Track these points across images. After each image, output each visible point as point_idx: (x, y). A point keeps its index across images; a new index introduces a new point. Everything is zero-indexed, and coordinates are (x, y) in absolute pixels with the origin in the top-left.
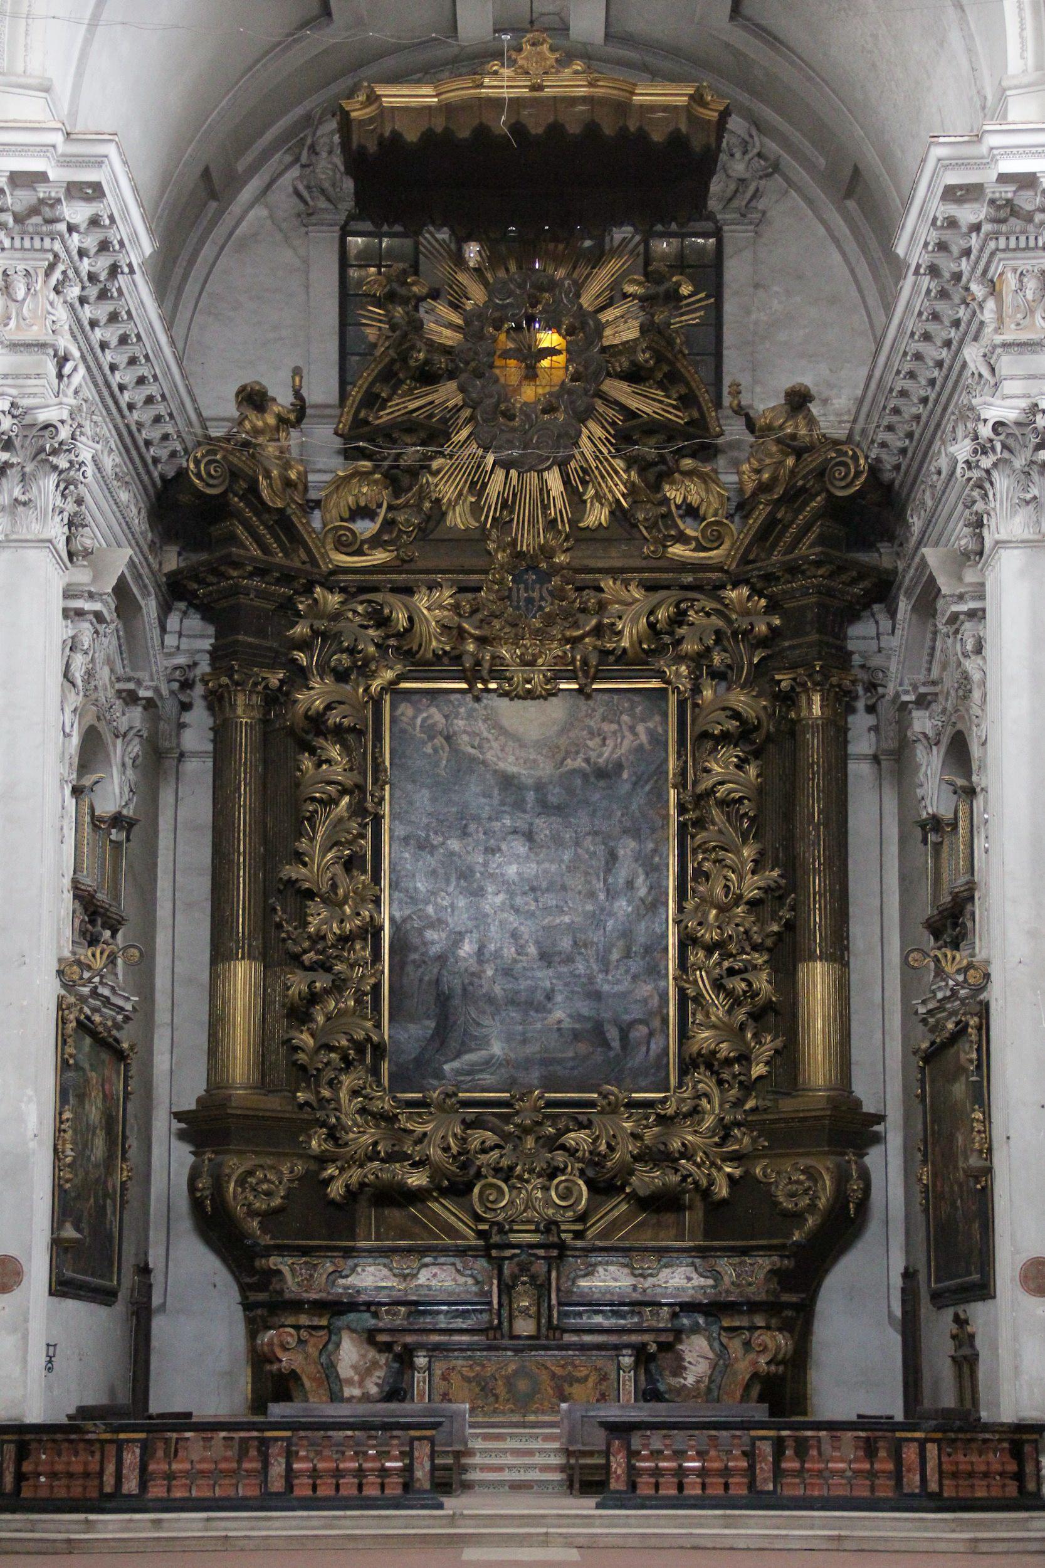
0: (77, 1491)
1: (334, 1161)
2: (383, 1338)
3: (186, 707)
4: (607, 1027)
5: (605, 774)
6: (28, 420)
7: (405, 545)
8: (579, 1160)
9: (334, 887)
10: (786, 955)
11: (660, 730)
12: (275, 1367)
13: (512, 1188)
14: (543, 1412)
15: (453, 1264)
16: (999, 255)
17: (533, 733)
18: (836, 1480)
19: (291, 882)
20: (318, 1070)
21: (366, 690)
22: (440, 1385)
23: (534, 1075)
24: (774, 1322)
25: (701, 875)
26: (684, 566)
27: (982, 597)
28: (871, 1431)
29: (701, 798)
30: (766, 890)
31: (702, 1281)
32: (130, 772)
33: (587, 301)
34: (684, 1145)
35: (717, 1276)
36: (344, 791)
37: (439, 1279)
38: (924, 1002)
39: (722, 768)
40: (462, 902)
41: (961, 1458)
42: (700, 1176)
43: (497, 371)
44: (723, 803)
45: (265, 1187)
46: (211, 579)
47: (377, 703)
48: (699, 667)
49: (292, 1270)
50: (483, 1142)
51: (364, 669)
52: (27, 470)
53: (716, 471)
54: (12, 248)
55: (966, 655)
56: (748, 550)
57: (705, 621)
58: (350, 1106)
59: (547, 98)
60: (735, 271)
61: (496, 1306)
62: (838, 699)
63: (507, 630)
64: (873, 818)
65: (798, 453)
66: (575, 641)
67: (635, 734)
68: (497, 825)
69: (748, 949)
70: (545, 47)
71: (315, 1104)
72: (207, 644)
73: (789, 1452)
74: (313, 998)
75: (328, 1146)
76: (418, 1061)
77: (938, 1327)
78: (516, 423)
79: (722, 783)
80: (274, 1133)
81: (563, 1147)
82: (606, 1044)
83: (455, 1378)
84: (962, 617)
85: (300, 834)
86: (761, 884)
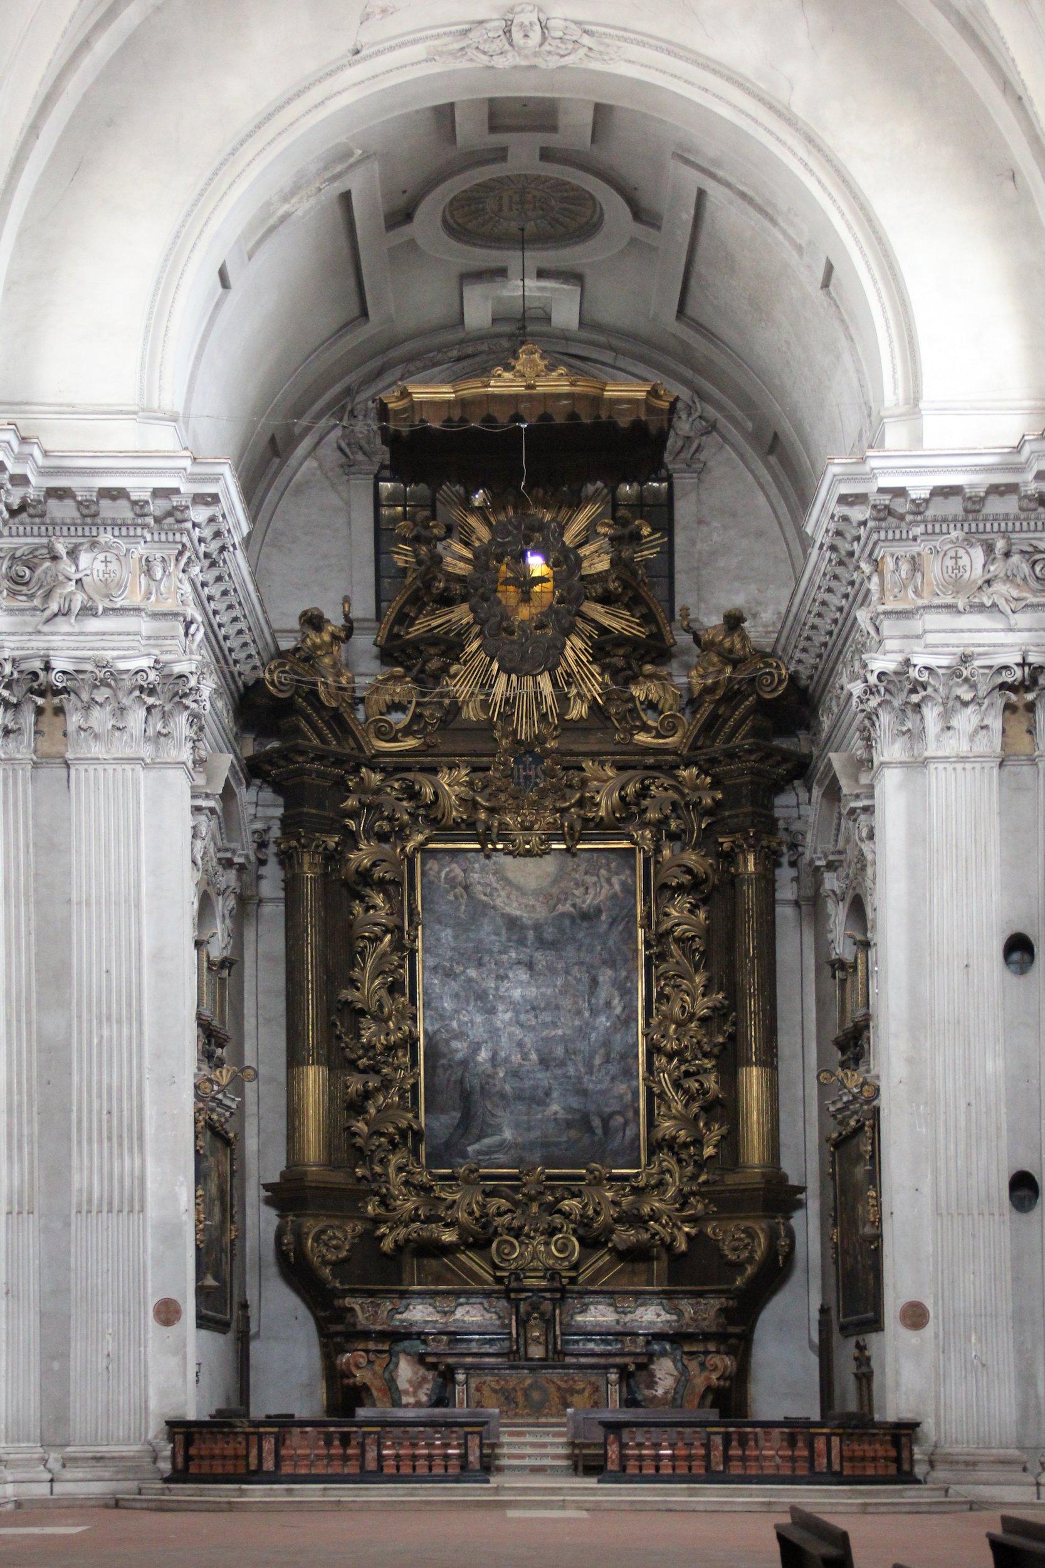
0: (230, 1469)
1: (385, 1222)
2: (430, 1359)
3: (262, 862)
5: (588, 916)
6: (166, 671)
7: (431, 734)
9: (381, 1007)
10: (729, 1060)
11: (630, 881)
13: (521, 1243)
14: (552, 1416)
16: (881, 544)
17: (532, 883)
18: (767, 1463)
19: (347, 1003)
21: (403, 849)
23: (537, 1156)
24: (722, 1348)
25: (663, 997)
26: (646, 750)
27: (872, 797)
28: (795, 1430)
29: (662, 937)
30: (714, 1009)
31: (668, 1317)
32: (228, 921)
33: (568, 538)
35: (680, 1313)
36: (386, 932)
37: (470, 1315)
38: (834, 1103)
39: (677, 910)
40: (479, 1019)
41: (856, 1447)
42: (665, 1233)
43: (499, 595)
46: (282, 763)
48: (659, 831)
49: (362, 1308)
51: (400, 834)
53: (670, 674)
54: (153, 541)
55: (862, 840)
56: (696, 738)
57: (664, 794)
58: (397, 1179)
59: (539, 395)
60: (684, 510)
62: (767, 857)
64: (794, 949)
65: (735, 664)
66: (563, 811)
68: (505, 957)
70: (537, 356)
72: (279, 812)
73: (734, 1443)
74: (367, 1095)
75: (381, 1211)
76: (448, 1145)
77: (845, 1352)
78: (515, 637)
79: (678, 925)
80: (340, 1200)
81: (560, 1212)
82: (591, 1130)
83: (486, 1391)
85: (353, 965)
86: (710, 1004)
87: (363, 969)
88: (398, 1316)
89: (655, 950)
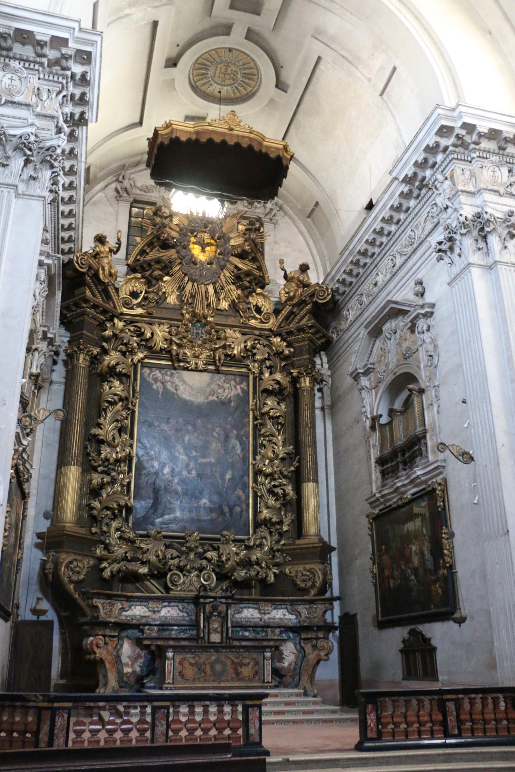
1: (106, 560)
4: (224, 507)
5: (224, 403)
6: (41, 145)
7: (151, 307)
8: (212, 564)
9: (114, 439)
10: (298, 479)
11: (246, 388)
12: (92, 656)
13: (184, 575)
14: (228, 681)
15: (178, 606)
19: (95, 436)
20: (102, 518)
21: (132, 360)
22: (179, 668)
29: (263, 415)
44: (271, 418)
45: (78, 569)
46: (74, 308)
47: (135, 366)
49: (103, 606)
50: (172, 555)
51: (132, 352)
52: (37, 167)
63: (189, 343)
67: (236, 389)
71: (99, 533)
72: (66, 339)
74: (102, 486)
76: (145, 518)
80: (83, 544)
81: (206, 558)
82: (222, 513)
83: (186, 664)
84: (421, 316)
85: (99, 417)
86: (286, 451)
88: (124, 613)
89: (259, 421)
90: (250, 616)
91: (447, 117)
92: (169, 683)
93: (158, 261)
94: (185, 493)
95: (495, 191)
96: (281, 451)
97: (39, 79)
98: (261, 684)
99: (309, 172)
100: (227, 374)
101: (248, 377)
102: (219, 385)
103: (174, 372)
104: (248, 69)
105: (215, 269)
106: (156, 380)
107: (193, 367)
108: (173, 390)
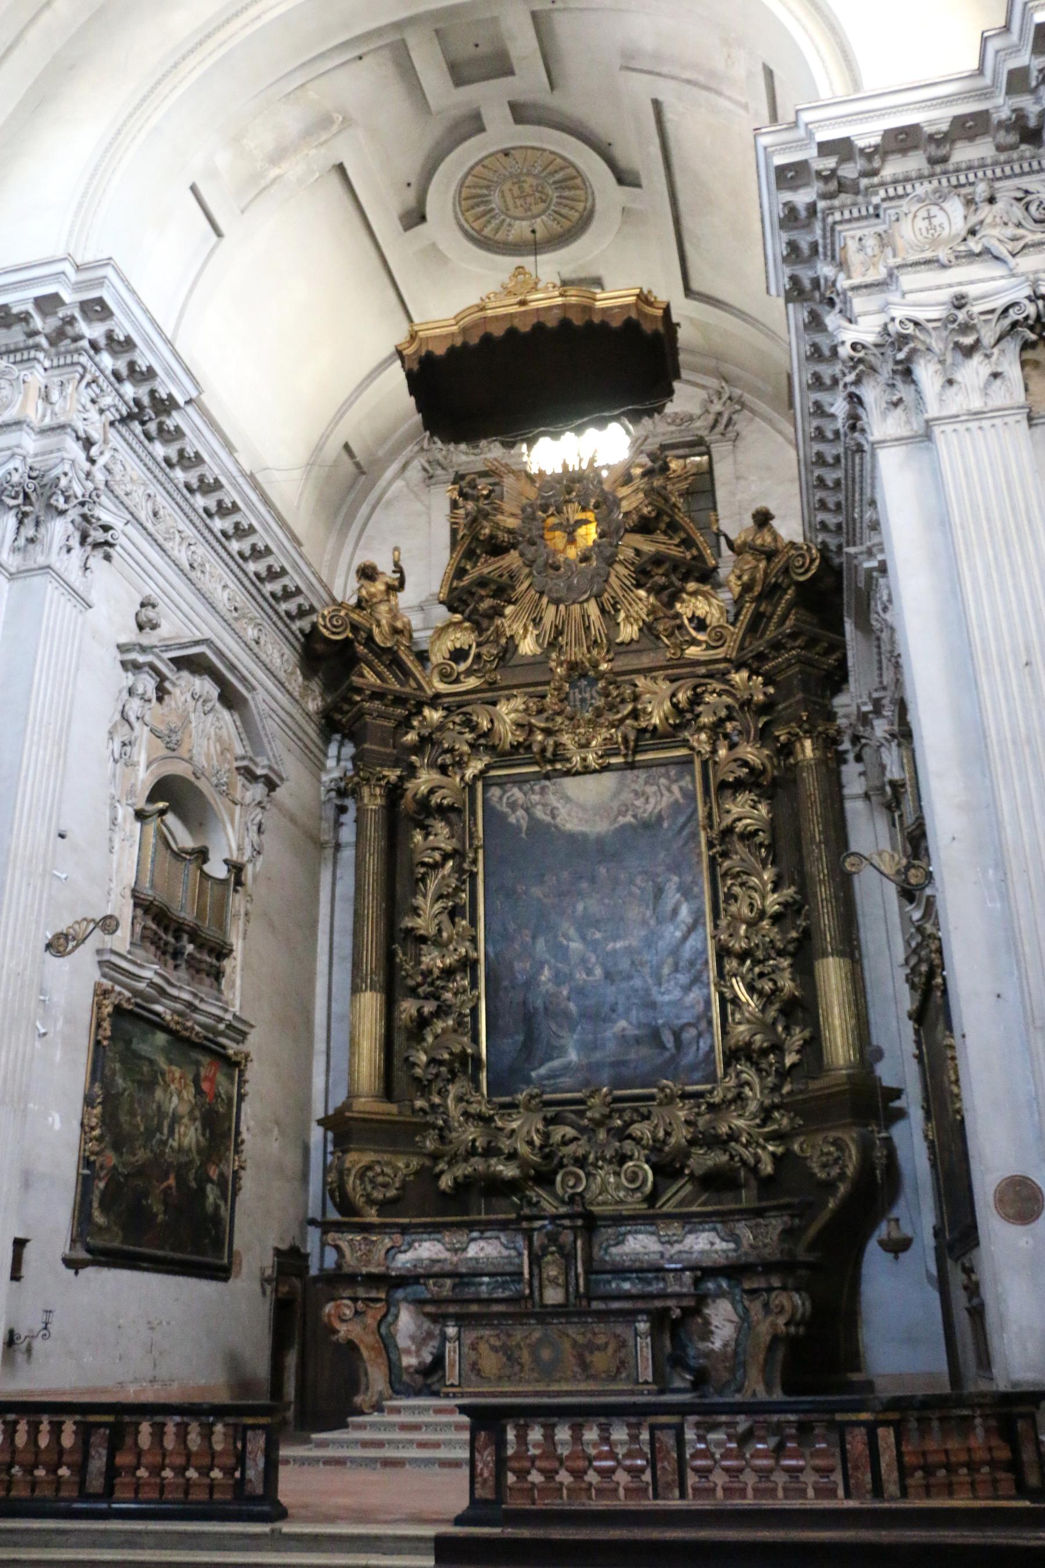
5: (649, 826)
7: (490, 671)
8: (644, 1147)
10: (803, 955)
11: (690, 787)
14: (567, 1380)
15: (498, 1238)
21: (462, 779)
23: (606, 1075)
24: (790, 1282)
30: (785, 905)
31: (724, 1245)
34: (730, 1128)
35: (734, 1238)
46: (346, 707)
47: (471, 787)
48: (717, 734)
51: (461, 764)
61: (527, 1276)
69: (773, 955)
79: (740, 819)
81: (630, 1137)
82: (662, 1047)
83: (483, 1348)
85: (414, 894)
86: (780, 900)
87: (425, 896)
89: (718, 848)
90: (641, 1250)
91: (785, 147)
92: (452, 1385)
93: (482, 582)
94: (584, 1015)
95: (927, 262)
96: (772, 903)
97: (45, 369)
98: (630, 1387)
99: (755, 320)
100: (651, 767)
101: (692, 762)
102: (636, 793)
103: (547, 783)
104: (556, 172)
105: (597, 568)
106: (513, 806)
107: (579, 767)
108: (548, 819)
